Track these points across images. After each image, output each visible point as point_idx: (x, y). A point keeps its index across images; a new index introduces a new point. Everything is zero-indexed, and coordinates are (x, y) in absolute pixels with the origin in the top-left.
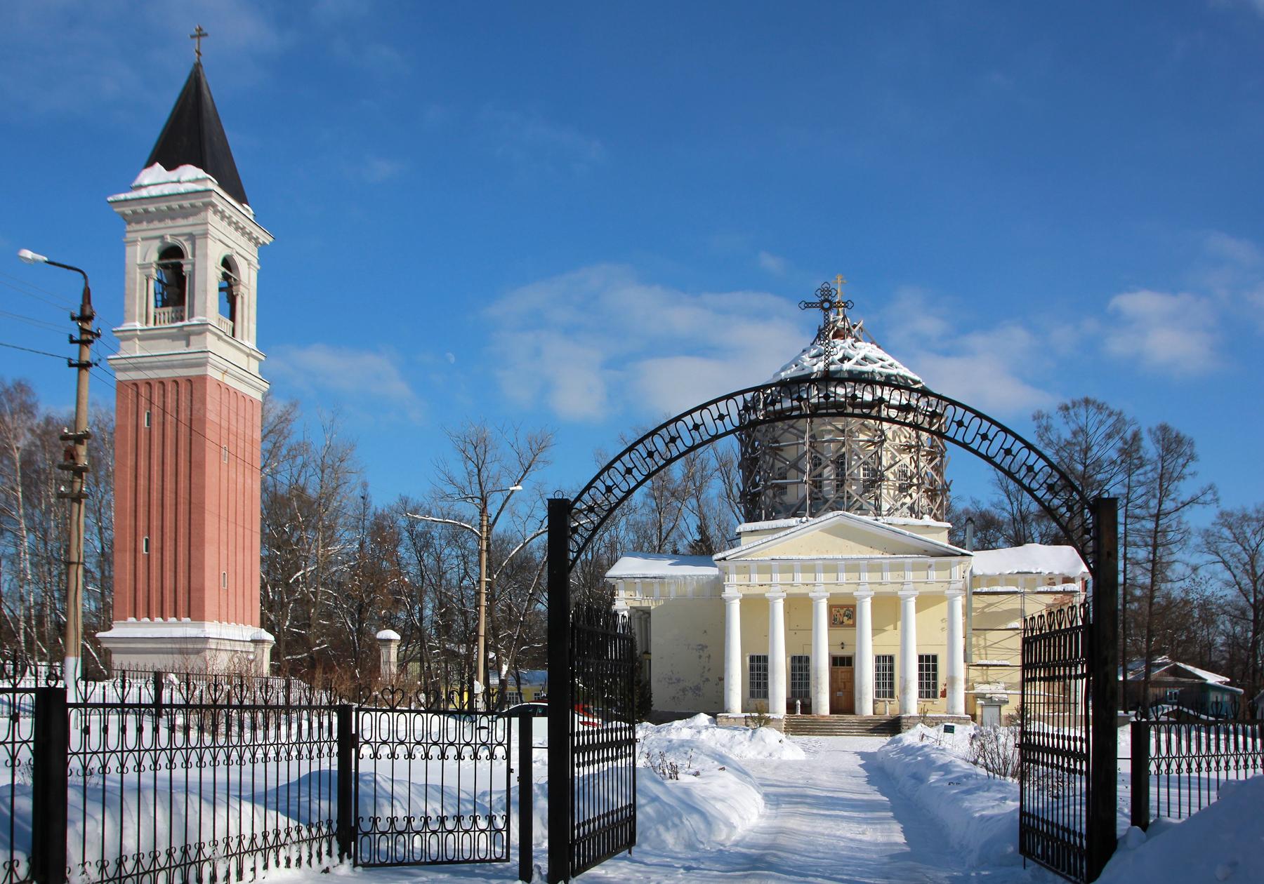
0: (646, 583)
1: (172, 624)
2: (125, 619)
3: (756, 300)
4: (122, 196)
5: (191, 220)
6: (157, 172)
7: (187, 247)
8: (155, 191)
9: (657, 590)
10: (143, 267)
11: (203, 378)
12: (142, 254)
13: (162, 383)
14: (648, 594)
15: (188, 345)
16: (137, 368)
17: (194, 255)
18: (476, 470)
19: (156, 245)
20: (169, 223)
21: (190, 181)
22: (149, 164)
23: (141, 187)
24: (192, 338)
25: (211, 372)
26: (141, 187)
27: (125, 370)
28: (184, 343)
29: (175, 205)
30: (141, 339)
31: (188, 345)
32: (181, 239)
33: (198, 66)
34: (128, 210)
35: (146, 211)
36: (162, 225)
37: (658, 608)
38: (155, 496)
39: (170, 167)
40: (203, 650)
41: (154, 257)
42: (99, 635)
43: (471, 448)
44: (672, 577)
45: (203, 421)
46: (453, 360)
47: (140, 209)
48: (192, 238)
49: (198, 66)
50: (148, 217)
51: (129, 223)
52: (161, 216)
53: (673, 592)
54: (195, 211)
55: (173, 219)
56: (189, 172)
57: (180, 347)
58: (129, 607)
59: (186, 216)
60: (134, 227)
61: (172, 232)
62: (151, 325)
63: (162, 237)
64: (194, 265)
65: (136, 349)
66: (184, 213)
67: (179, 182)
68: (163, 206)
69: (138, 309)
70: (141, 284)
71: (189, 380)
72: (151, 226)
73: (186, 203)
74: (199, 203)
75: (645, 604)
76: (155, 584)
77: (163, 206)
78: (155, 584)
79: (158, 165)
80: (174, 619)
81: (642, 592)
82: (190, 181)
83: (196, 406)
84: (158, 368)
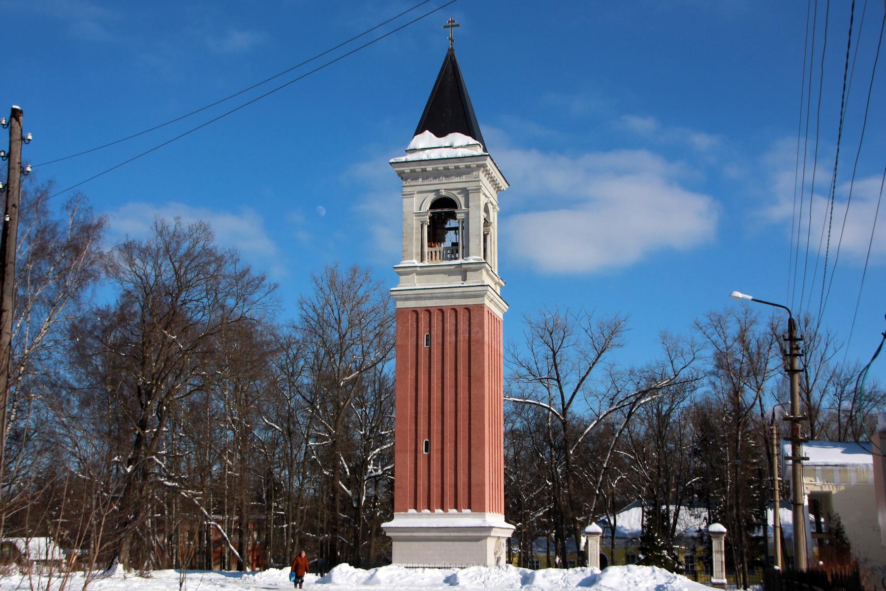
0: (827, 470)
1: (453, 515)
2: (406, 511)
3: (623, 158)
4: (403, 159)
5: (464, 178)
6: (427, 138)
7: (461, 199)
8: (423, 156)
9: (837, 476)
10: (418, 214)
11: (481, 307)
12: (417, 204)
13: (441, 310)
14: (828, 480)
15: (464, 279)
16: (418, 298)
17: (467, 206)
18: (551, 353)
19: (431, 197)
20: (444, 180)
21: (461, 147)
22: (420, 131)
23: (415, 150)
24: (468, 274)
25: (487, 302)
26: (415, 150)
27: (407, 299)
28: (460, 277)
29: (451, 166)
30: (418, 274)
31: (464, 279)
32: (454, 192)
33: (451, 50)
34: (407, 170)
35: (424, 170)
36: (437, 181)
37: (839, 493)
38: (436, 404)
39: (440, 134)
40: (486, 537)
41: (427, 206)
42: (384, 525)
43: (547, 334)
44: (853, 465)
45: (481, 343)
46: (323, 212)
47: (418, 169)
48: (465, 192)
49: (451, 50)
50: (425, 175)
51: (406, 180)
52: (436, 174)
53: (853, 479)
54: (468, 170)
55: (447, 176)
56: (459, 139)
57: (456, 281)
58: (410, 499)
59: (459, 175)
60: (410, 182)
61: (447, 187)
62: (426, 263)
63: (437, 191)
64: (467, 214)
65: (416, 283)
66: (458, 172)
67: (451, 147)
68: (441, 167)
69: (415, 249)
70: (417, 228)
71: (468, 309)
72: (426, 182)
73: (462, 165)
74: (473, 165)
75: (826, 489)
76: (435, 481)
77: (441, 167)
78: (435, 481)
79: (427, 131)
80: (455, 511)
81: (822, 479)
82: (461, 147)
83: (474, 330)
84: (437, 298)
